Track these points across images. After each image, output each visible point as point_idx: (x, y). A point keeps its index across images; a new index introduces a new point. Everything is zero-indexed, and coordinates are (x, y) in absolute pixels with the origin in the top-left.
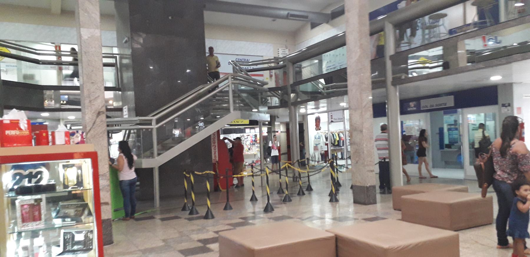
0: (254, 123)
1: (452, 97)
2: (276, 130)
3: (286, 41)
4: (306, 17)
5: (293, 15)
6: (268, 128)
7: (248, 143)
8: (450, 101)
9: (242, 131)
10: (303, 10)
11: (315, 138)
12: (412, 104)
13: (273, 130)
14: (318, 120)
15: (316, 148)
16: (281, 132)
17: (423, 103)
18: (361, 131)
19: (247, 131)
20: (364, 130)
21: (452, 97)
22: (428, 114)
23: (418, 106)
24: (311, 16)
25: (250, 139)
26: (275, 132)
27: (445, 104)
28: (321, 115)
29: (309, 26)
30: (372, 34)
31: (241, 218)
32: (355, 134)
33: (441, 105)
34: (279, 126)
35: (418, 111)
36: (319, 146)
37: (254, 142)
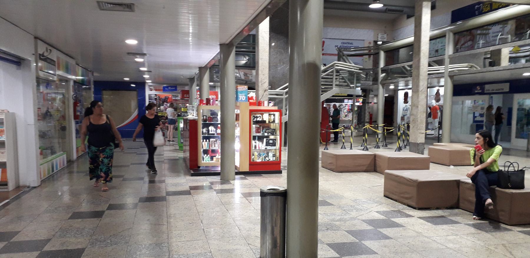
0: (350, 96)
1: (508, 84)
2: (370, 101)
3: (385, 27)
4: (402, 11)
5: (390, 10)
6: (363, 100)
7: (345, 111)
8: (506, 87)
9: (342, 101)
10: (397, 4)
11: (403, 110)
12: (478, 88)
13: (367, 101)
14: (406, 95)
15: (403, 118)
16: (375, 103)
17: (487, 87)
18: (418, 107)
19: (346, 101)
20: (419, 107)
21: (508, 84)
22: (501, 95)
23: (483, 89)
24: (406, 10)
25: (347, 107)
26: (368, 103)
27: (503, 89)
28: (440, 88)
29: (405, 16)
30: (430, 40)
31: (387, 238)
32: (414, 108)
33: (499, 90)
34: (373, 98)
35: (482, 93)
36: (406, 117)
37: (351, 110)
